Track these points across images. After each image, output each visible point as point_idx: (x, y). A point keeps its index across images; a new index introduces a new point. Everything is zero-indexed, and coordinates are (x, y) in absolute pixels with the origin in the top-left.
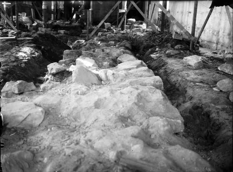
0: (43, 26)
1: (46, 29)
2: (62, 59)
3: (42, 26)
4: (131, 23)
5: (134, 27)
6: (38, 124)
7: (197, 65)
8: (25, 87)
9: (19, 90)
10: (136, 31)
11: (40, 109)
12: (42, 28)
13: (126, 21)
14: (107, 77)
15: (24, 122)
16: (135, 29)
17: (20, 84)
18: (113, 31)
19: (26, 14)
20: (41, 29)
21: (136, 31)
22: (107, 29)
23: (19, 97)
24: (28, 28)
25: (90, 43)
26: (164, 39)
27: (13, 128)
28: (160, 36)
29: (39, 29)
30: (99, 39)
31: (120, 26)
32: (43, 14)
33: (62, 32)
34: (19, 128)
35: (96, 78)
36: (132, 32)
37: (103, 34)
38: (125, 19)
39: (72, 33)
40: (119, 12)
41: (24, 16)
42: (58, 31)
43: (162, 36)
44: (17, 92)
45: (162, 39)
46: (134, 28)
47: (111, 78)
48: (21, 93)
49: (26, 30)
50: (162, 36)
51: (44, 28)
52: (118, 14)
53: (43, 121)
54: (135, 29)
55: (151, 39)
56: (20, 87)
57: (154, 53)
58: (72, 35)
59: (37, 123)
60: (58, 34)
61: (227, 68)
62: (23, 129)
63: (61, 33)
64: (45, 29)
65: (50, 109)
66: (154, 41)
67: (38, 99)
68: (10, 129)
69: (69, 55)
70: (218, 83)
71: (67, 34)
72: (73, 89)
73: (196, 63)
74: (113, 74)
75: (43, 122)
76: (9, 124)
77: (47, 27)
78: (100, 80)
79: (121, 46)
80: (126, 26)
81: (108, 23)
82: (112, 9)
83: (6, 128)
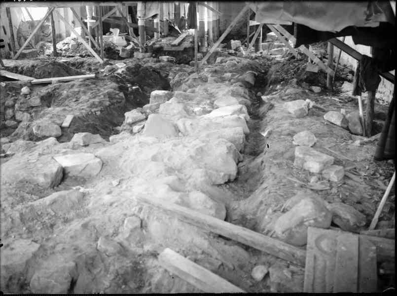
0: (140, 50)
1: (143, 54)
2: (149, 103)
3: (139, 50)
4: (272, 39)
5: (275, 46)
6: (96, 174)
7: (299, 113)
8: (90, 140)
9: (84, 142)
10: (277, 53)
11: (98, 160)
12: (138, 53)
13: (261, 37)
14: (185, 128)
15: (83, 172)
16: (276, 49)
17: (85, 136)
18: (242, 53)
19: (119, 30)
20: (138, 55)
21: (277, 53)
22: (234, 50)
23: (84, 149)
24: (120, 54)
25: (194, 77)
26: (301, 69)
27: (74, 176)
28: (297, 64)
29: (135, 54)
30: (210, 71)
31: (251, 45)
32: (139, 33)
33: (165, 58)
34: (79, 177)
35: (173, 128)
36: (271, 55)
37: (223, 59)
38: (260, 33)
39: (180, 60)
40: (250, 25)
41: (116, 36)
42: (159, 58)
43: (299, 65)
44: (82, 144)
45: (298, 69)
46: (274, 48)
47: (189, 128)
48: (86, 146)
49: (117, 56)
50: (299, 65)
51: (142, 52)
52: (248, 28)
53: (101, 171)
54: (276, 49)
55: (283, 70)
56: (85, 140)
57: (274, 93)
58: (179, 63)
59: (95, 173)
60: (159, 61)
61: (332, 116)
62: (83, 178)
63: (163, 61)
64: (142, 54)
65: (109, 161)
66: (287, 72)
67: (101, 151)
68: (71, 177)
69: (156, 98)
70: (294, 136)
71: (171, 61)
72: (53, 150)
73: (296, 111)
74: (191, 124)
75: (101, 172)
76: (71, 173)
77: (146, 52)
78: (178, 130)
79: (238, 80)
80: (262, 45)
81: (237, 41)
82: (229, 27)
83: (68, 176)
